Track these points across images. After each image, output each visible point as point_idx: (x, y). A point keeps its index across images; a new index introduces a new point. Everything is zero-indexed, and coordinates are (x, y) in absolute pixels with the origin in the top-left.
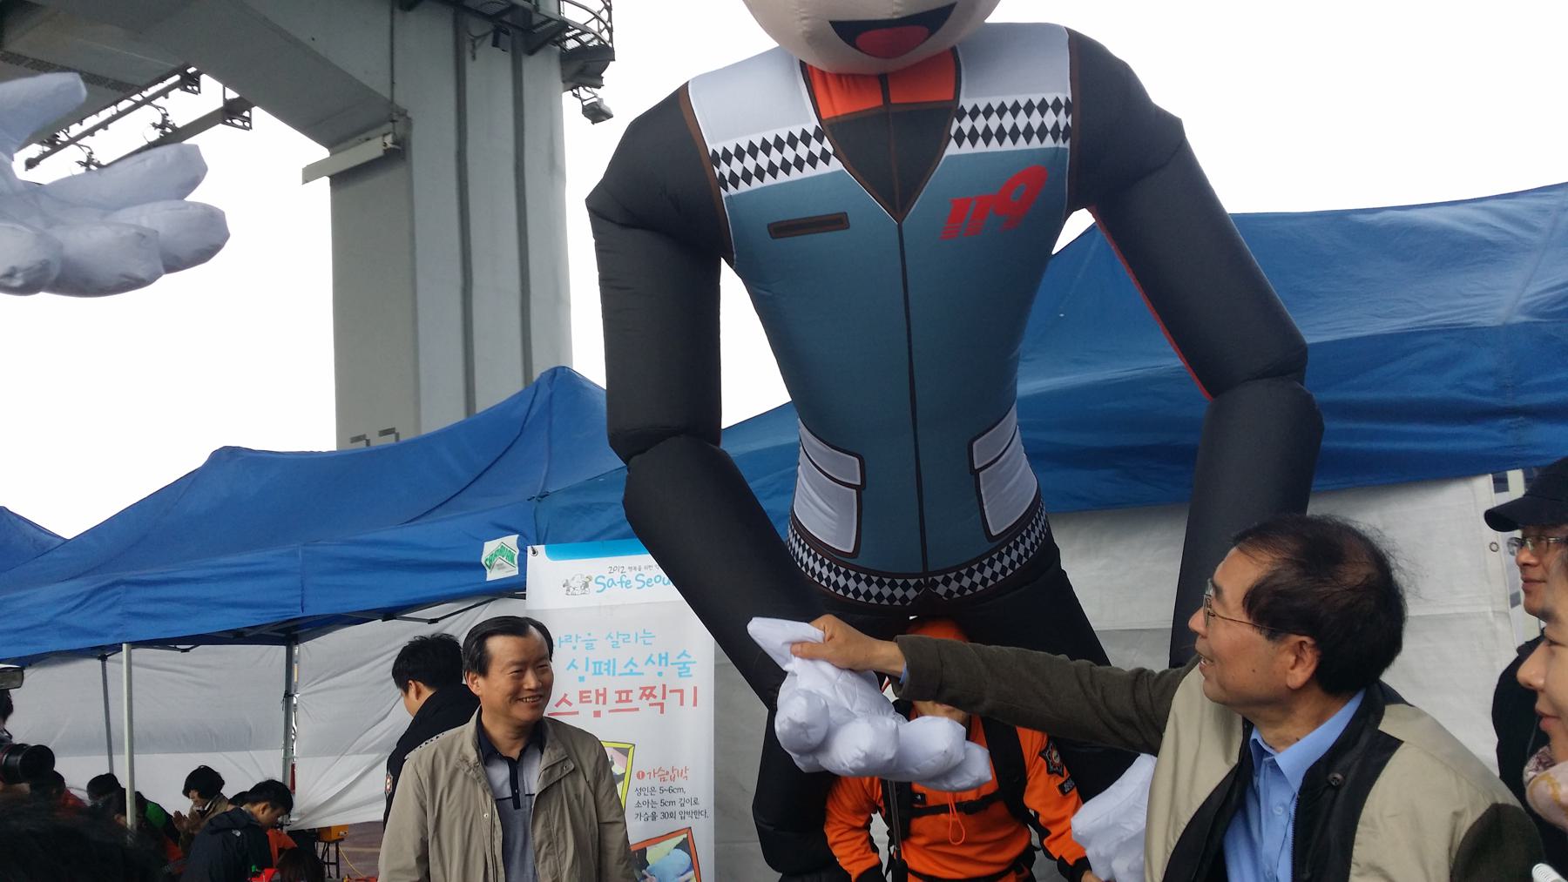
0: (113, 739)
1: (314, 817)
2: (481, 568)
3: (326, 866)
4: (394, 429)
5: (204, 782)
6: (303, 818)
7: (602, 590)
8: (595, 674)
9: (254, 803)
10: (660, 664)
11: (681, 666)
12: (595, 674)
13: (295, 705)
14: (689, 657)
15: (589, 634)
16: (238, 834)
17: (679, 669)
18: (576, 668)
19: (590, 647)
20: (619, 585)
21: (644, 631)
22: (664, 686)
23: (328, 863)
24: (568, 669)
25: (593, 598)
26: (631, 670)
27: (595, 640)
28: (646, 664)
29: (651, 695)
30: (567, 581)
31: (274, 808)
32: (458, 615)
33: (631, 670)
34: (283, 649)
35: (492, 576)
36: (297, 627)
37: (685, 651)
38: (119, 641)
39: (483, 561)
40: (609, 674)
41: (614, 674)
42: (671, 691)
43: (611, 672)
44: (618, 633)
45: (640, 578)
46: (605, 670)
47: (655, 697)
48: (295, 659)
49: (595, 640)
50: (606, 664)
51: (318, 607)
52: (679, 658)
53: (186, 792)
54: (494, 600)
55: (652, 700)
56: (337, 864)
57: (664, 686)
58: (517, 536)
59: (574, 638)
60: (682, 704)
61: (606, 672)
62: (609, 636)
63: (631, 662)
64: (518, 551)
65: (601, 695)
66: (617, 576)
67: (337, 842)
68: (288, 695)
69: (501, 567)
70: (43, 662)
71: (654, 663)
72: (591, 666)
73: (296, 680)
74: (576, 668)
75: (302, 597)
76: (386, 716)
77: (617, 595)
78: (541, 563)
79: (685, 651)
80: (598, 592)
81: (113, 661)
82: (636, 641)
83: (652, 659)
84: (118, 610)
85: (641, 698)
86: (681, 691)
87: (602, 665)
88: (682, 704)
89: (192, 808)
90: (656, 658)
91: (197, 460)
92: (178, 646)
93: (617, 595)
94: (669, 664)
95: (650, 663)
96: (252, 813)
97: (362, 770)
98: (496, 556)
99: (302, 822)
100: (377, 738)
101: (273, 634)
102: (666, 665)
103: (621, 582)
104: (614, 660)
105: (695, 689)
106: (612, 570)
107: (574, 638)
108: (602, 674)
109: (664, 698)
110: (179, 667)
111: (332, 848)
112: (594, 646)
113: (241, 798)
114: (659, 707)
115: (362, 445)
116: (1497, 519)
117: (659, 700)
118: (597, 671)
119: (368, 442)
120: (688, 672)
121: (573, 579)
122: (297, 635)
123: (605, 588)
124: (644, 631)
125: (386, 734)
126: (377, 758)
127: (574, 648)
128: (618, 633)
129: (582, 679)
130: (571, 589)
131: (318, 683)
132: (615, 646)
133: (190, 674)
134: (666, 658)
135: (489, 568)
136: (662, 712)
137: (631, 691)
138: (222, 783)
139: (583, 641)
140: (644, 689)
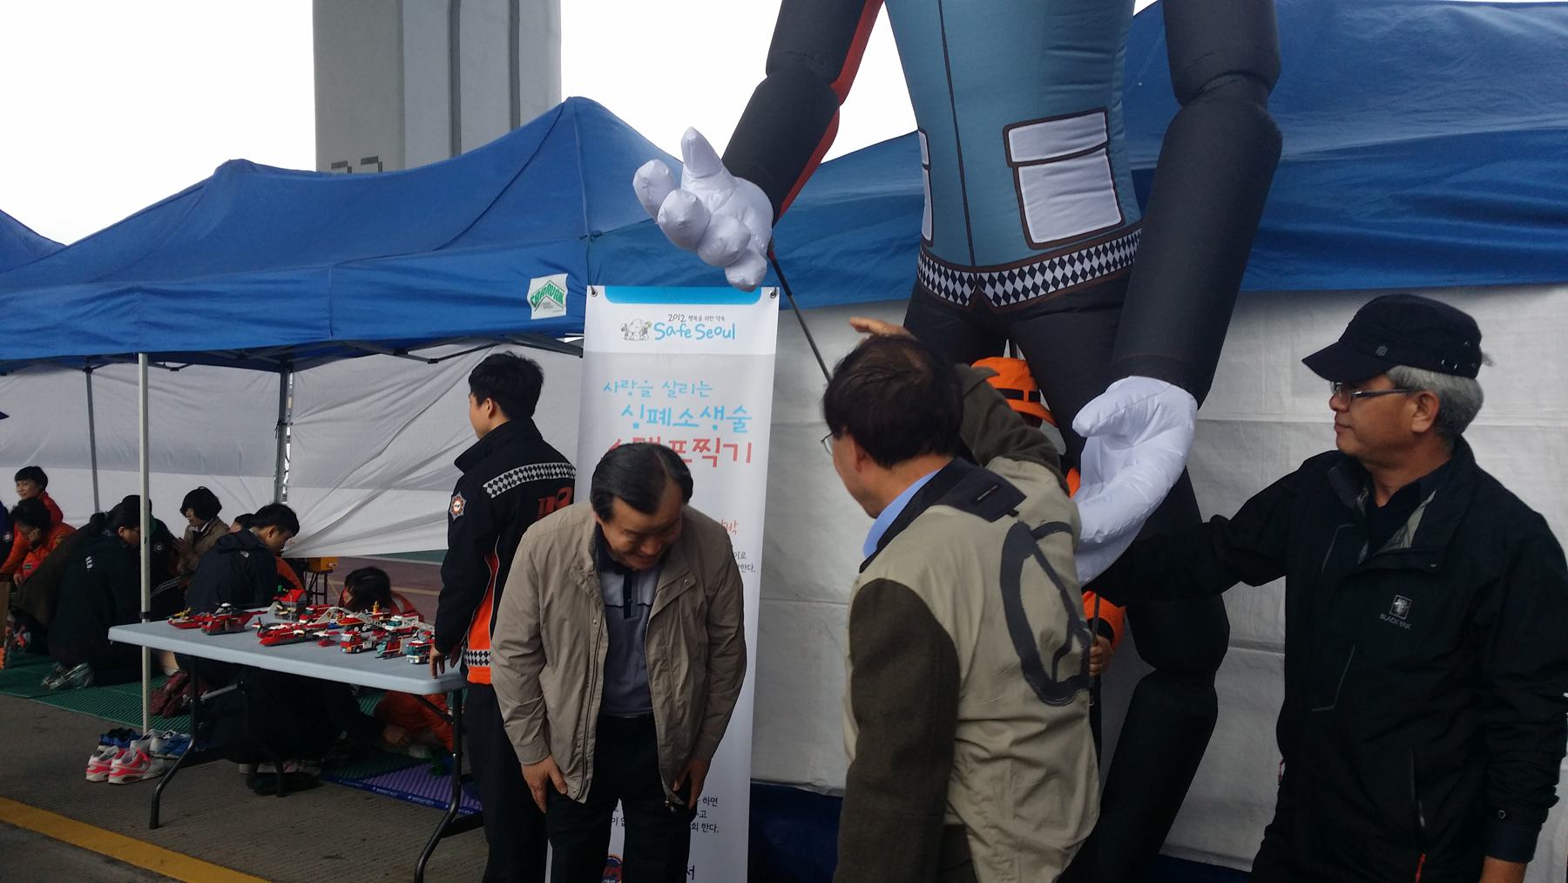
0: (97, 453)
1: (303, 547)
2: (525, 305)
3: (314, 596)
4: (377, 158)
5: (201, 504)
6: (293, 547)
7: (702, 338)
8: (649, 421)
9: (262, 526)
10: (716, 417)
11: (736, 421)
12: (649, 421)
13: (289, 437)
14: (745, 412)
15: (646, 382)
16: (247, 555)
17: (735, 423)
18: (631, 414)
19: (646, 394)
20: (679, 333)
21: (702, 382)
22: (718, 440)
23: (317, 594)
24: (623, 414)
25: (650, 345)
26: (686, 421)
27: (652, 388)
28: (702, 416)
29: (705, 448)
30: (626, 325)
31: (281, 531)
32: (461, 356)
33: (686, 421)
34: (277, 376)
35: (537, 314)
36: (293, 356)
37: (741, 407)
38: (134, 350)
39: (529, 298)
40: (664, 423)
41: (669, 424)
42: (725, 446)
43: (666, 422)
44: (675, 382)
45: (700, 328)
46: (660, 419)
47: (709, 450)
48: (289, 393)
49: (652, 388)
50: (661, 413)
51: (347, 332)
52: (735, 412)
53: (184, 510)
54: (498, 344)
55: (705, 453)
56: (325, 594)
57: (718, 440)
58: (565, 276)
59: (630, 384)
60: (735, 459)
61: (661, 421)
62: (666, 384)
63: (686, 413)
64: (566, 291)
65: (700, 448)
66: (676, 324)
67: (326, 573)
68: (282, 424)
69: (547, 306)
70: (25, 369)
71: (709, 416)
72: (646, 414)
73: (290, 406)
74: (631, 414)
75: (331, 321)
76: (380, 453)
77: (675, 344)
78: (601, 307)
79: (741, 407)
80: (657, 339)
81: (99, 374)
82: (693, 392)
83: (708, 411)
84: (133, 318)
85: (694, 450)
86: (735, 447)
87: (658, 414)
88: (735, 459)
89: (187, 530)
90: (711, 411)
91: (205, 171)
92: (167, 364)
93: (675, 344)
94: (725, 419)
95: (705, 416)
96: (260, 537)
97: (355, 505)
98: (543, 294)
99: (293, 551)
100: (371, 474)
101: (272, 360)
102: (722, 419)
103: (681, 331)
104: (670, 410)
105: (750, 445)
106: (672, 318)
107: (630, 384)
108: (657, 422)
109: (718, 451)
110: (165, 386)
111: (321, 581)
112: (650, 394)
113: (244, 520)
114: (712, 460)
115: (372, 169)
116: (1320, 363)
117: (712, 453)
118: (652, 419)
119: (350, 170)
120: (744, 427)
121: (632, 324)
122: (291, 363)
123: (664, 335)
124: (702, 382)
125: (379, 472)
126: (372, 493)
127: (630, 394)
128: (675, 382)
129: (636, 426)
130: (630, 334)
131: (309, 415)
132: (672, 394)
133: (174, 393)
134: (722, 412)
135: (535, 306)
136: (715, 465)
137: (685, 442)
138: (219, 507)
139: (639, 388)
140: (699, 441)
